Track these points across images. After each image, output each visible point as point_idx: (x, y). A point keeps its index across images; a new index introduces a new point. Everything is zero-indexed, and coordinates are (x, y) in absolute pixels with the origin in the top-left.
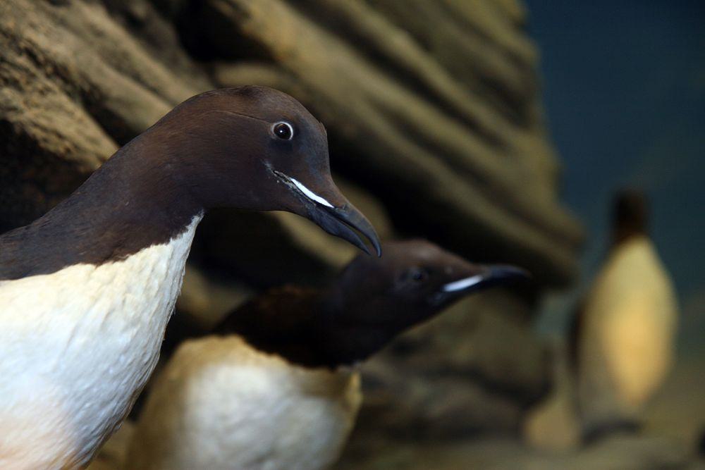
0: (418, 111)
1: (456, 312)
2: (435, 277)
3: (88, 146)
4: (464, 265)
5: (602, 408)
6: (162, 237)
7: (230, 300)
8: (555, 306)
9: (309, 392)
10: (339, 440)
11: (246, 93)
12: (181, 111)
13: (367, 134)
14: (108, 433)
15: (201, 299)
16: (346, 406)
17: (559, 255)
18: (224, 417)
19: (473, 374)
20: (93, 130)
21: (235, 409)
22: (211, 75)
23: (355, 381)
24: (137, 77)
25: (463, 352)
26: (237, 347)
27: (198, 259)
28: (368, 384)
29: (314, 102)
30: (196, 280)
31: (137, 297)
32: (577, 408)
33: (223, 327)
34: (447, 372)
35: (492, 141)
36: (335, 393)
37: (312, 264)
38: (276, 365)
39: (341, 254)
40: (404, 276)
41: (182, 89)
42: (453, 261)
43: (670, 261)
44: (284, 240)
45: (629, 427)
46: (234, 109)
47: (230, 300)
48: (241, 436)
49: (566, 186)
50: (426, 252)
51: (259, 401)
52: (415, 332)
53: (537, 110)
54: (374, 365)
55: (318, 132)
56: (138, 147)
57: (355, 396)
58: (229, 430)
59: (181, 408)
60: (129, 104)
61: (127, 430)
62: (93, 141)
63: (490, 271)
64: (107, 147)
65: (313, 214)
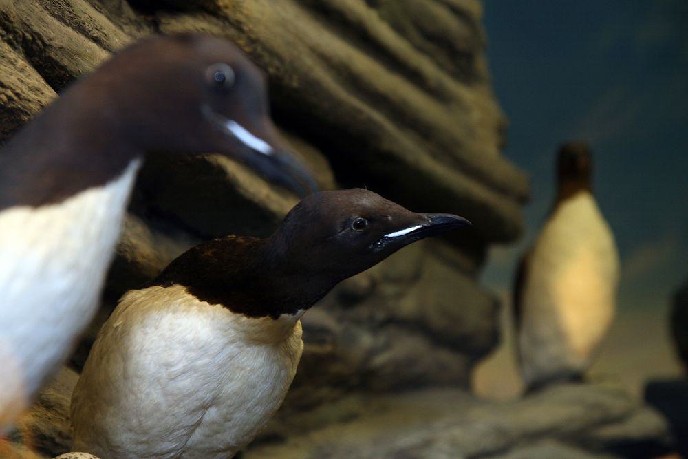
0: (363, 63)
1: (402, 261)
2: (376, 224)
3: (31, 95)
4: (408, 213)
5: (545, 359)
6: (100, 179)
7: (173, 250)
8: (500, 257)
9: (253, 340)
10: (283, 387)
11: (185, 39)
12: (119, 58)
13: (313, 85)
14: (48, 379)
15: (146, 248)
16: (290, 354)
17: (505, 207)
18: (168, 365)
19: (418, 325)
20: (36, 79)
21: (178, 357)
22: (155, 25)
23: (299, 329)
24: (80, 28)
25: (408, 305)
26: (180, 293)
27: (139, 206)
28: (312, 333)
29: (258, 51)
30: (140, 229)
31: (75, 243)
32: (520, 359)
33: (165, 278)
34: (394, 322)
35: (437, 94)
36: (277, 341)
37: (259, 214)
38: (219, 312)
39: (282, 204)
40: (345, 224)
41: (120, 38)
42: (393, 209)
43: (607, 211)
44: (229, 188)
45: (576, 377)
46: (172, 54)
47: (173, 250)
48: (185, 383)
49: (508, 140)
50: (368, 199)
51: (203, 349)
52: (361, 280)
53: (481, 64)
54: (316, 315)
55: (256, 78)
56: (76, 93)
57: (298, 344)
58: (173, 378)
59: (126, 358)
60: (72, 54)
61: (73, 377)
62: (35, 90)
63: (430, 219)
64: (49, 94)
65: (249, 159)
